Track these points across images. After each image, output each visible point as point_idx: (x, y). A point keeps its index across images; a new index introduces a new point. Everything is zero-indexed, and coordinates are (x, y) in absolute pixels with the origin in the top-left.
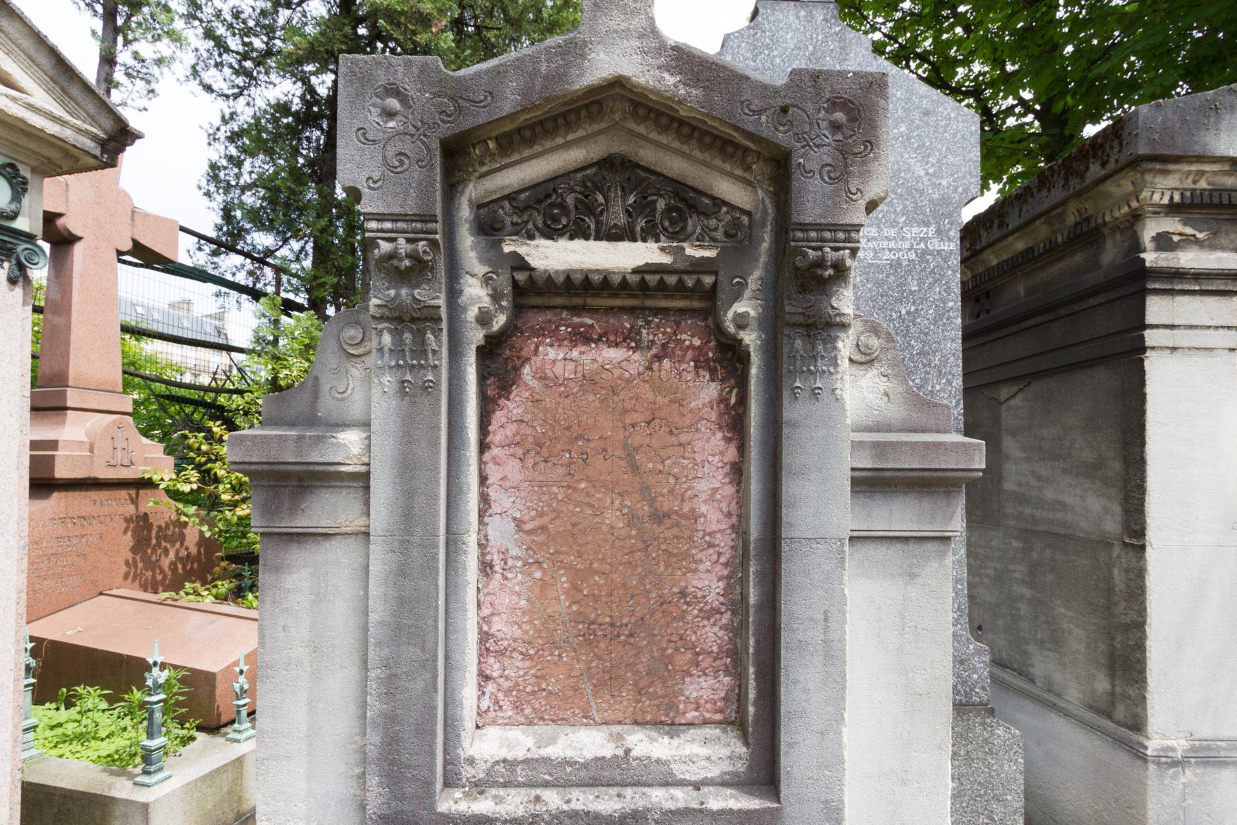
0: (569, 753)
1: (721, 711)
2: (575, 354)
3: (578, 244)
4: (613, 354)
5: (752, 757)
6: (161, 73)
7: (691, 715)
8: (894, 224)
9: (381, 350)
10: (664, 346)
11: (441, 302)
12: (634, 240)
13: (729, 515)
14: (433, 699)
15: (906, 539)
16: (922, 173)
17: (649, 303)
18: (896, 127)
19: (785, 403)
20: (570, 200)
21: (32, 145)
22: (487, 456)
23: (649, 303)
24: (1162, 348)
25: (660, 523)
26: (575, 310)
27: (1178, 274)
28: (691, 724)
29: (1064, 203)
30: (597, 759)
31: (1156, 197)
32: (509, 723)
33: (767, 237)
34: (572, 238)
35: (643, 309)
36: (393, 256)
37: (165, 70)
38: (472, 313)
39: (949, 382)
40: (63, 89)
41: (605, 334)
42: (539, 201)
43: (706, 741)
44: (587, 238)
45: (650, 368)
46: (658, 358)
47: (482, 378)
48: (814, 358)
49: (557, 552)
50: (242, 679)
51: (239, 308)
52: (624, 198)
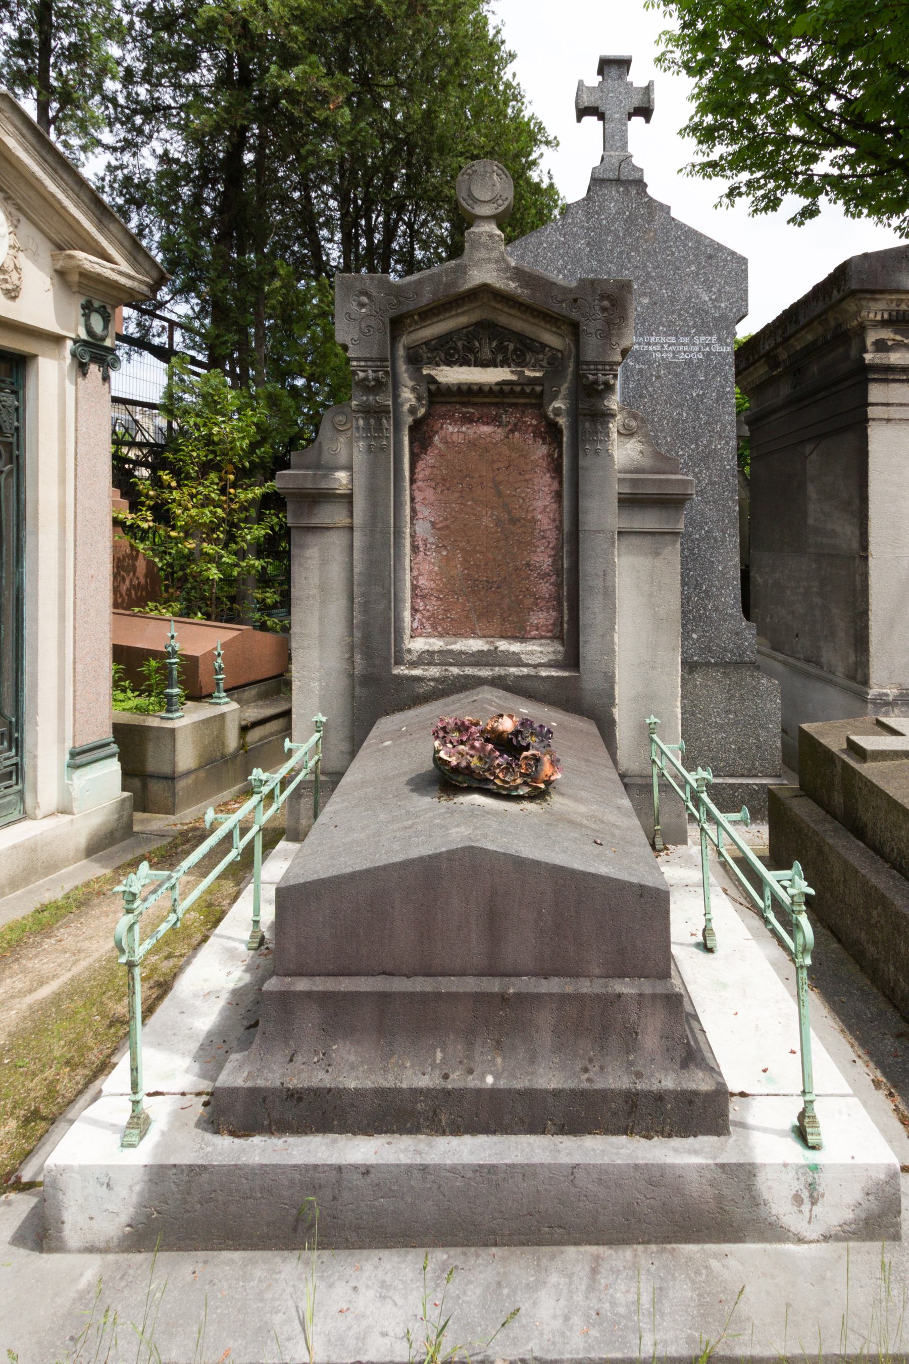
0: (463, 648)
1: (551, 631)
2: (464, 429)
3: (464, 369)
4: (486, 429)
5: (566, 651)
6: (87, 158)
7: (534, 633)
8: (687, 334)
9: (358, 428)
10: (515, 425)
11: (390, 403)
12: (496, 366)
13: (554, 520)
14: (389, 615)
15: (652, 534)
16: (707, 299)
17: (506, 400)
18: (689, 267)
19: (580, 457)
20: (460, 344)
21: (115, 293)
22: (414, 486)
23: (506, 400)
24: (881, 419)
25: (514, 524)
26: (464, 404)
27: (890, 369)
28: (534, 638)
29: (825, 312)
30: (479, 651)
31: (872, 316)
32: (429, 636)
33: (571, 365)
34: (461, 366)
35: (503, 404)
36: (366, 379)
37: (90, 154)
38: (406, 407)
39: (727, 443)
40: (135, 259)
41: (481, 418)
42: (442, 346)
43: (541, 645)
44: (469, 366)
45: (507, 437)
46: (512, 431)
47: (411, 443)
48: (596, 432)
49: (455, 541)
50: (219, 660)
51: (129, 360)
52: (490, 344)
